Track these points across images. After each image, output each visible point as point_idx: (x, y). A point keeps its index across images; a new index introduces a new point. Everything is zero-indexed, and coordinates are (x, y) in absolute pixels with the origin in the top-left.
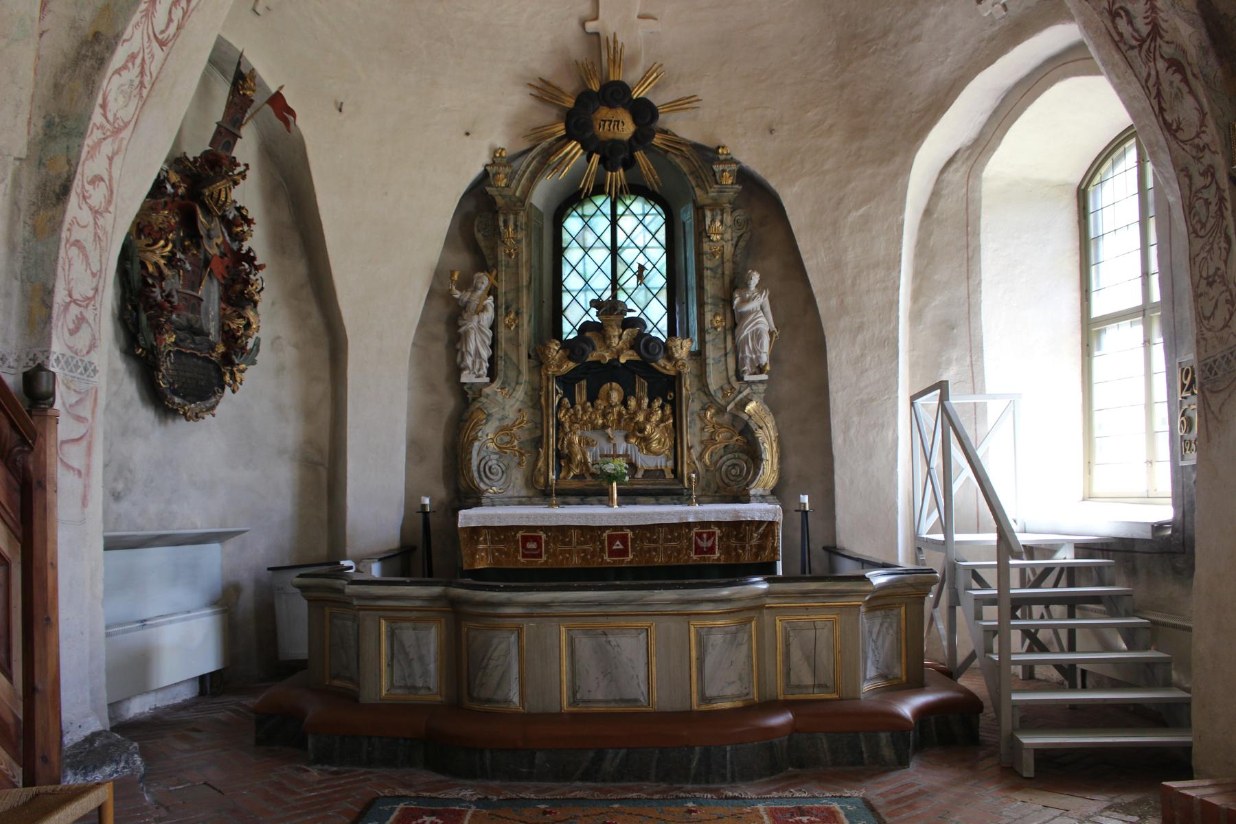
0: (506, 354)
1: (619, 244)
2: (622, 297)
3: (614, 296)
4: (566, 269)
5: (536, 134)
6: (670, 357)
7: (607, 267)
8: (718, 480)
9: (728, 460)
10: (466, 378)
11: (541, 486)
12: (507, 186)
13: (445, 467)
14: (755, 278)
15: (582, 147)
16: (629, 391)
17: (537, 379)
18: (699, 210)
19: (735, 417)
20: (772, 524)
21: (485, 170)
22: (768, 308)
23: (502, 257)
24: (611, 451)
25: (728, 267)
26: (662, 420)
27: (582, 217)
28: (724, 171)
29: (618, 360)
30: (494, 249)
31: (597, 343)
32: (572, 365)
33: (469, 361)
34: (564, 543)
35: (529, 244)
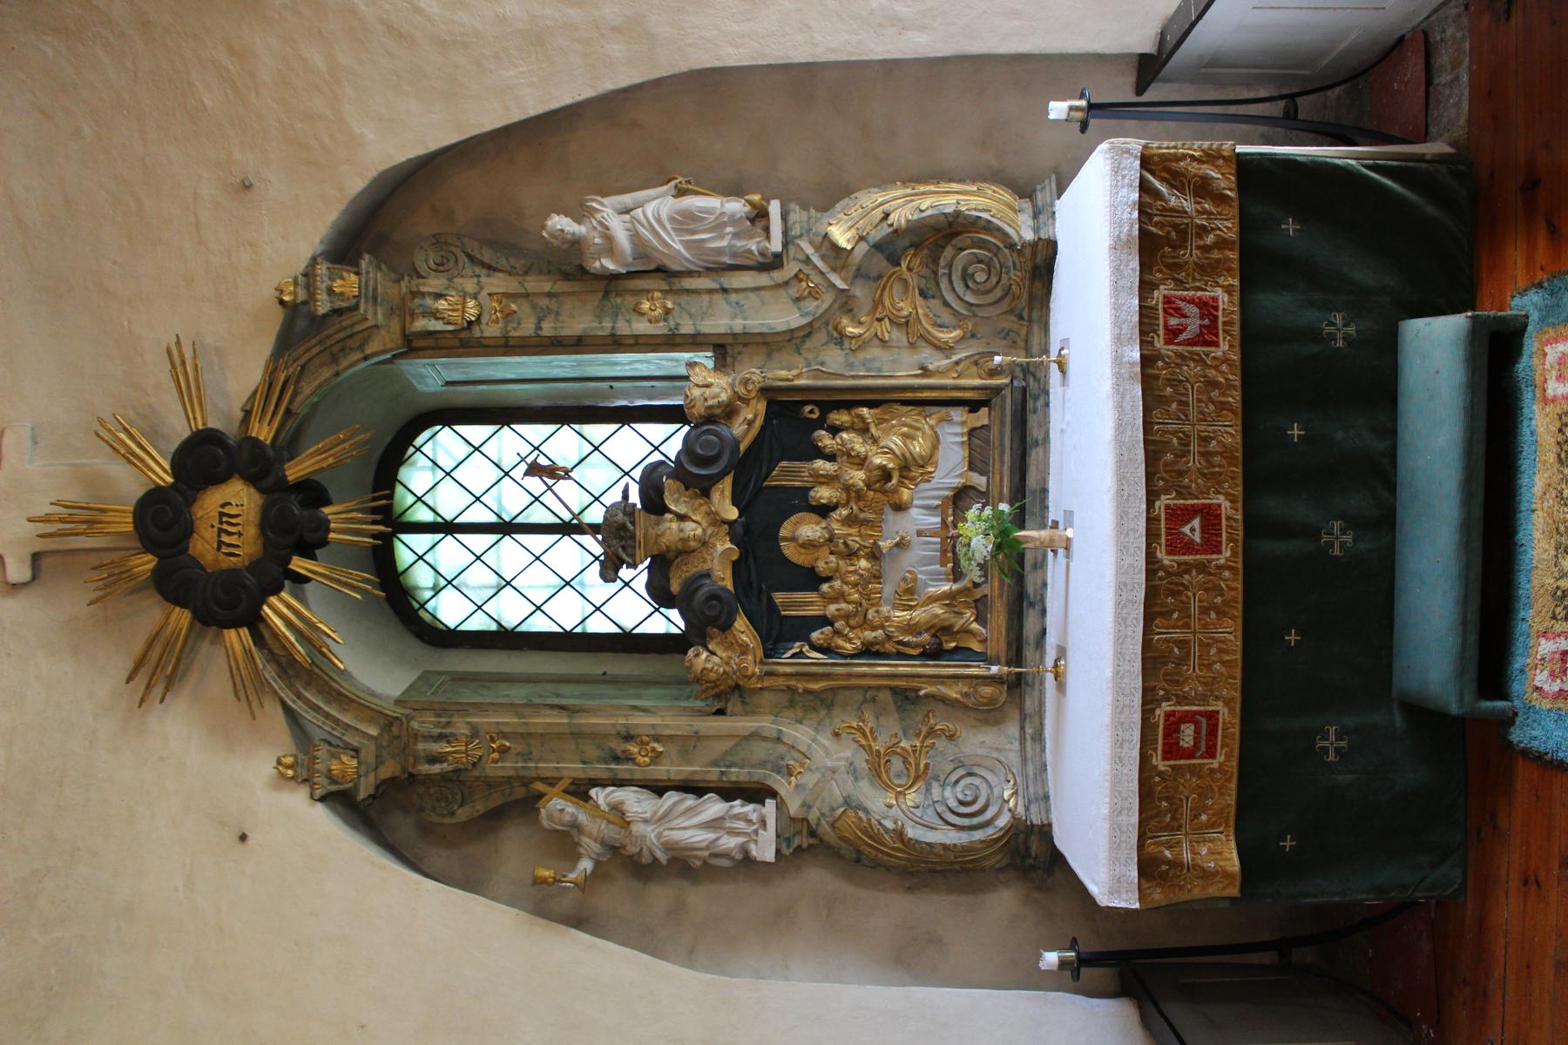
0: (715, 764)
1: (493, 519)
2: (595, 515)
3: (594, 529)
4: (539, 624)
5: (248, 688)
6: (729, 412)
7: (537, 542)
8: (993, 312)
9: (954, 292)
10: (765, 850)
11: (1002, 694)
12: (356, 751)
13: (950, 890)
14: (560, 223)
15: (276, 591)
16: (799, 501)
17: (768, 696)
18: (413, 345)
19: (860, 274)
20: (1146, 162)
21: (322, 799)
22: (627, 199)
23: (508, 766)
24: (916, 558)
25: (534, 284)
26: (864, 430)
27: (437, 590)
28: (330, 291)
29: (731, 523)
30: (490, 784)
31: (693, 568)
32: (741, 623)
33: (730, 843)
34: (1184, 659)
35: (481, 708)
